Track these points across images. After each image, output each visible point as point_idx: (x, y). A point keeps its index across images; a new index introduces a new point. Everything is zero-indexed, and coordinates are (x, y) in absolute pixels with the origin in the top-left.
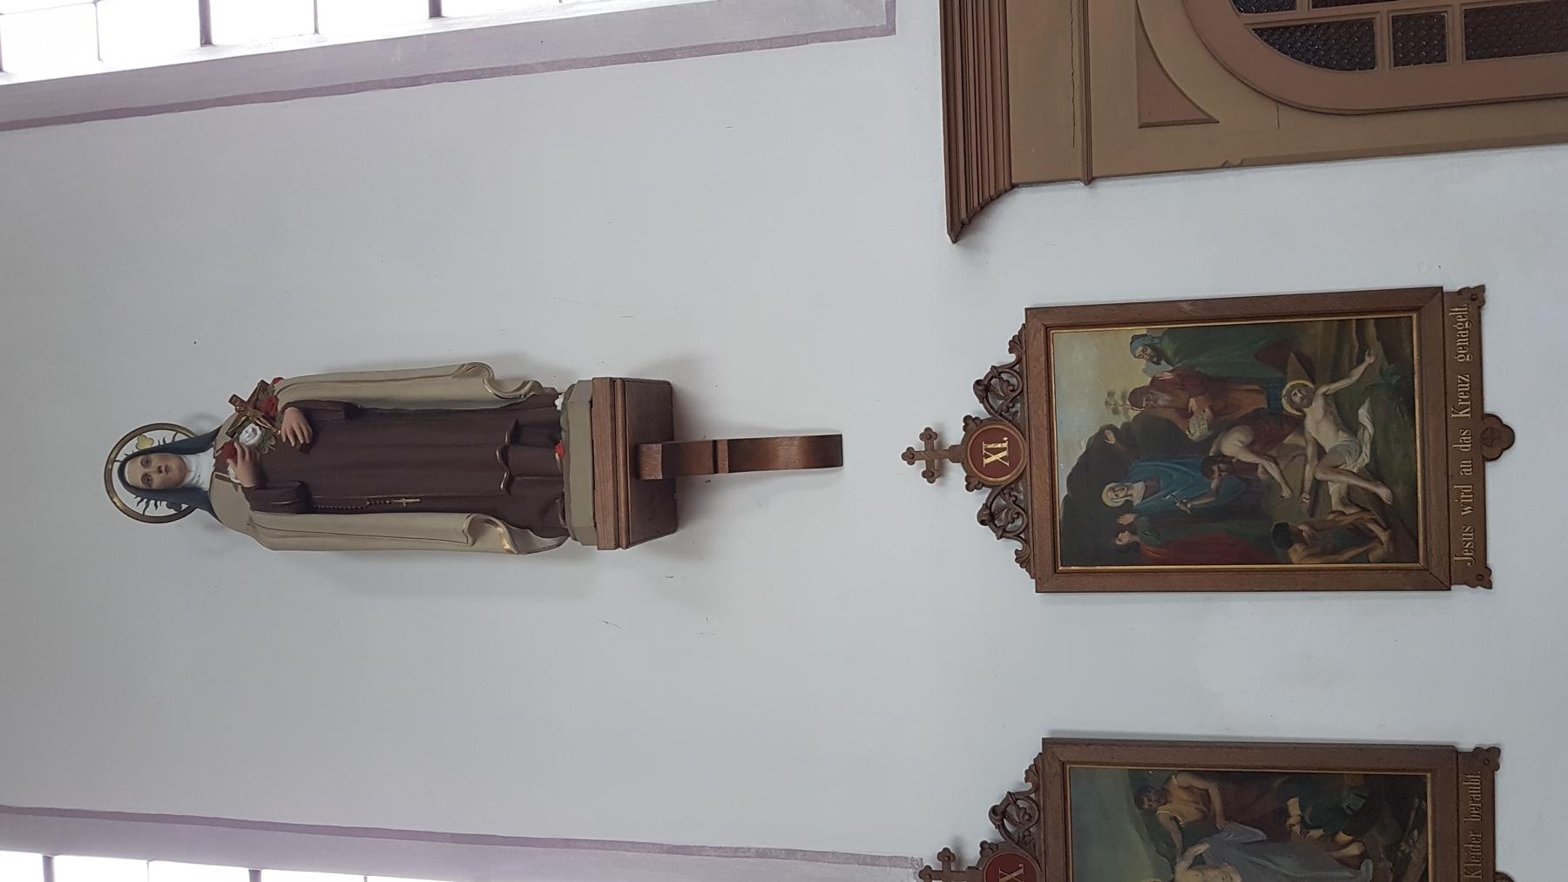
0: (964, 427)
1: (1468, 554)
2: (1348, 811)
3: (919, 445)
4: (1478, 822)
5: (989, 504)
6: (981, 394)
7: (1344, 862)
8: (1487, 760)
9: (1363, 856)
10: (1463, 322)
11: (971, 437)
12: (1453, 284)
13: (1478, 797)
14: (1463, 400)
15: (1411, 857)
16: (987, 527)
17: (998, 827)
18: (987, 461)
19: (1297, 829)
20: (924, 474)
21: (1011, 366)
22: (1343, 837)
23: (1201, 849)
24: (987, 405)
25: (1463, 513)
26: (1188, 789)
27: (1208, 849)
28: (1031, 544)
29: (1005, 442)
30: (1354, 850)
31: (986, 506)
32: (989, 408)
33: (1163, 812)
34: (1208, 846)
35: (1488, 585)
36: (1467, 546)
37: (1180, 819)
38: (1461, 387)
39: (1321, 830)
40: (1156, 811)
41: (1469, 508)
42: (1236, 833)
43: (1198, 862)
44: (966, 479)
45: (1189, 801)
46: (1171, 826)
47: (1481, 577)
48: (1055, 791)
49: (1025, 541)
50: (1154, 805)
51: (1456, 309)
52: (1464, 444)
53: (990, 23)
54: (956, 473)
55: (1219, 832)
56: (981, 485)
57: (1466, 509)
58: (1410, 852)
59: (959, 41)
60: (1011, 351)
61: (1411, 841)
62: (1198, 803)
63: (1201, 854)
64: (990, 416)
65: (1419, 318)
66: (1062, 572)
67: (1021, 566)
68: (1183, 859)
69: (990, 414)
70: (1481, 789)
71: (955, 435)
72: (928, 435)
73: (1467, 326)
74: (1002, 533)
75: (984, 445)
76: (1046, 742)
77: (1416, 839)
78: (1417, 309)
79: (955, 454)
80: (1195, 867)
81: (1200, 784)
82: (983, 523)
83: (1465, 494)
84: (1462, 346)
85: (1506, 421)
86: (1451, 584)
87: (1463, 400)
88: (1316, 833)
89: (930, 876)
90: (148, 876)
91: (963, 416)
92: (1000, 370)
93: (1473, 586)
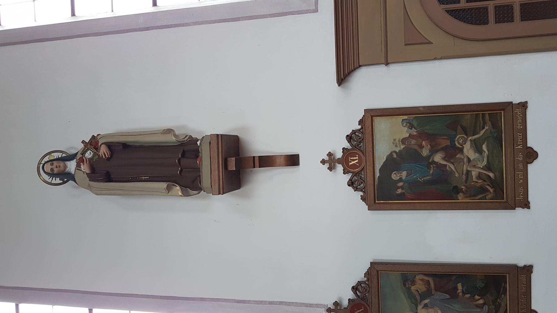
0: (343, 152)
1: (521, 197)
2: (479, 288)
3: (326, 158)
4: (525, 292)
5: (351, 179)
6: (348, 140)
7: (478, 306)
8: (528, 270)
9: (484, 304)
10: (520, 114)
11: (345, 155)
12: (516, 101)
13: (525, 283)
14: (520, 142)
15: (501, 304)
16: (351, 187)
17: (354, 293)
18: (351, 164)
19: (461, 294)
20: (328, 168)
21: (359, 130)
22: (477, 297)
23: (427, 301)
24: (351, 144)
25: (520, 182)
26: (422, 280)
27: (429, 301)
28: (366, 193)
29: (357, 157)
30: (481, 302)
31: (350, 180)
32: (351, 145)
33: (413, 288)
34: (429, 300)
35: (529, 208)
36: (521, 194)
37: (419, 291)
38: (519, 137)
39: (469, 295)
40: (411, 288)
41: (522, 180)
42: (439, 296)
43: (426, 306)
44: (343, 170)
45: (422, 284)
46: (416, 293)
47: (526, 205)
48: (375, 281)
49: (364, 192)
50: (410, 286)
51: (517, 110)
52: (520, 158)
53: (352, 8)
54: (340, 168)
55: (433, 295)
56: (348, 172)
57: (521, 181)
58: (501, 302)
59: (341, 14)
60: (359, 125)
61: (501, 298)
62: (425, 285)
63: (427, 303)
64: (352, 148)
65: (504, 113)
66: (377, 203)
67: (363, 201)
68: (420, 305)
69: (352, 147)
70: (526, 280)
71: (339, 154)
72: (330, 155)
73: (521, 116)
74: (356, 189)
75: (350, 158)
76: (372, 263)
77: (503, 298)
78: (503, 110)
79: (339, 161)
80: (425, 308)
81: (426, 278)
82: (349, 185)
83: (521, 175)
84: (519, 123)
85: (535, 149)
86: (515, 207)
87: (520, 142)
88: (468, 296)
89: (330, 311)
90: (53, 311)
91: (342, 148)
92: (355, 131)
93: (523, 208)
